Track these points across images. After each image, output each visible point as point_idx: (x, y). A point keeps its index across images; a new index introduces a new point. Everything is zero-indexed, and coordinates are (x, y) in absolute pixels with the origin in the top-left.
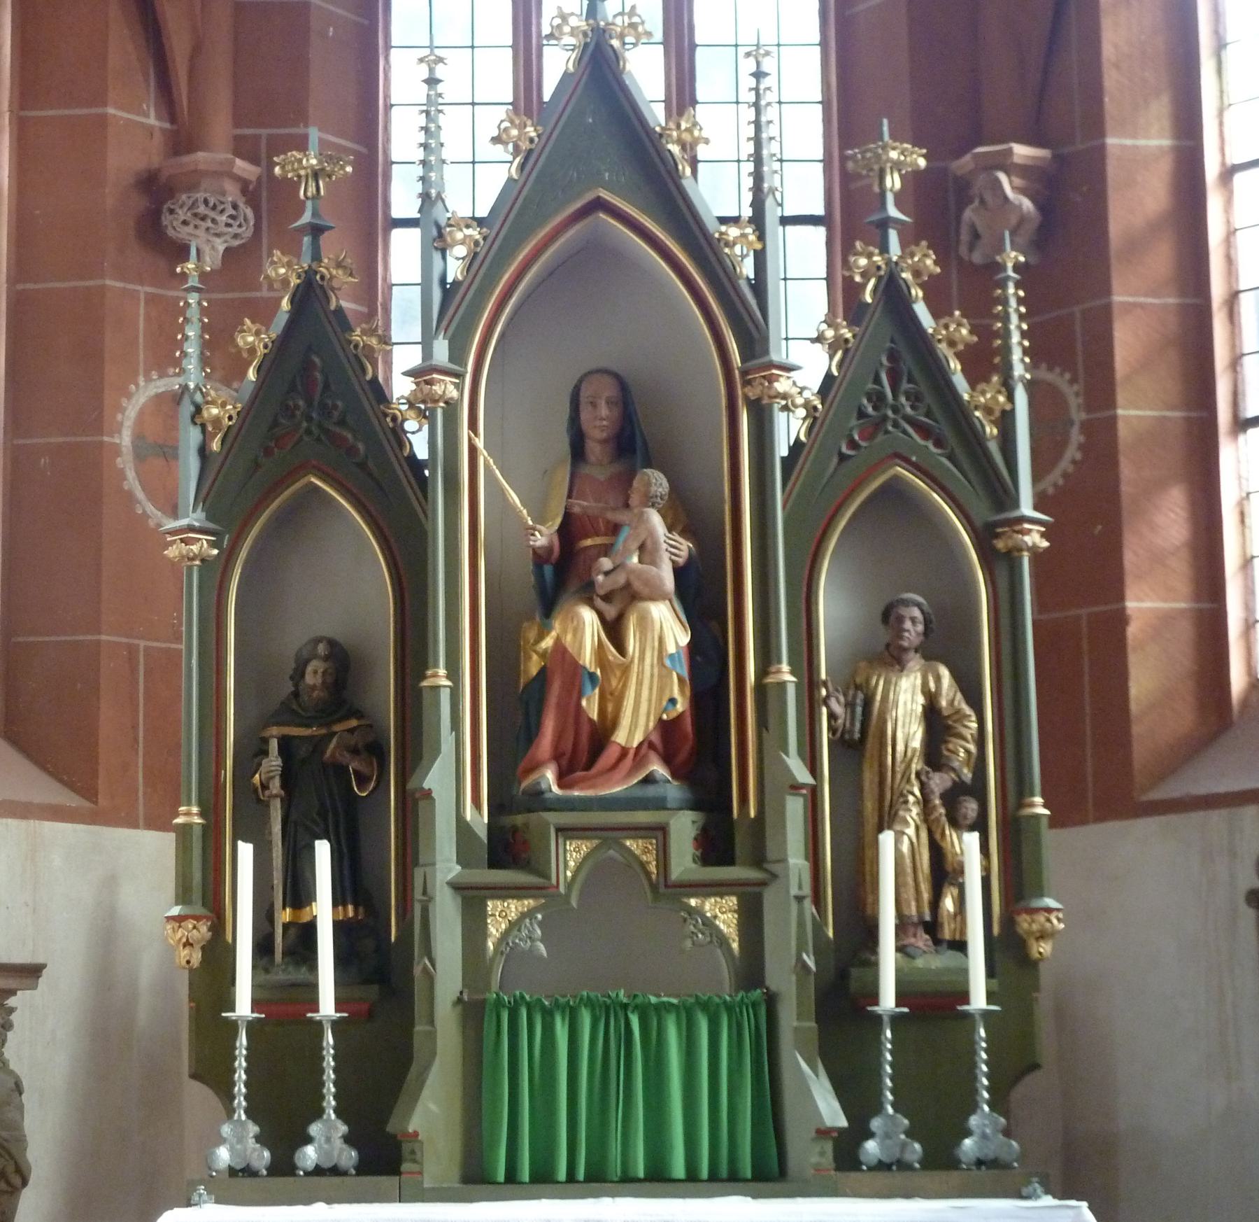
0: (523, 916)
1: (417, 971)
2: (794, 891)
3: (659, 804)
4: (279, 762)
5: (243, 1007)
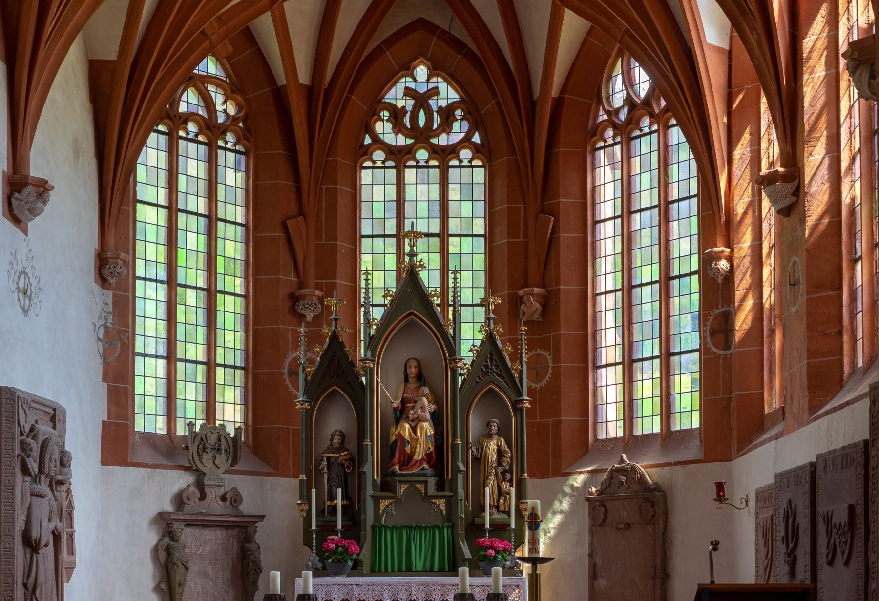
0: (389, 504)
1: (362, 518)
2: (459, 498)
3: (425, 475)
4: (326, 463)
5: (314, 527)
